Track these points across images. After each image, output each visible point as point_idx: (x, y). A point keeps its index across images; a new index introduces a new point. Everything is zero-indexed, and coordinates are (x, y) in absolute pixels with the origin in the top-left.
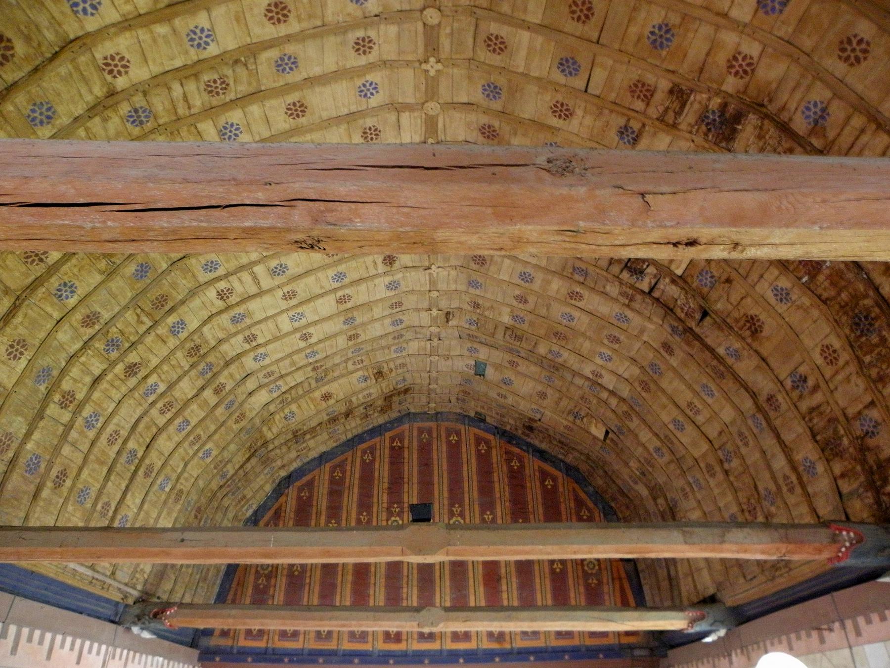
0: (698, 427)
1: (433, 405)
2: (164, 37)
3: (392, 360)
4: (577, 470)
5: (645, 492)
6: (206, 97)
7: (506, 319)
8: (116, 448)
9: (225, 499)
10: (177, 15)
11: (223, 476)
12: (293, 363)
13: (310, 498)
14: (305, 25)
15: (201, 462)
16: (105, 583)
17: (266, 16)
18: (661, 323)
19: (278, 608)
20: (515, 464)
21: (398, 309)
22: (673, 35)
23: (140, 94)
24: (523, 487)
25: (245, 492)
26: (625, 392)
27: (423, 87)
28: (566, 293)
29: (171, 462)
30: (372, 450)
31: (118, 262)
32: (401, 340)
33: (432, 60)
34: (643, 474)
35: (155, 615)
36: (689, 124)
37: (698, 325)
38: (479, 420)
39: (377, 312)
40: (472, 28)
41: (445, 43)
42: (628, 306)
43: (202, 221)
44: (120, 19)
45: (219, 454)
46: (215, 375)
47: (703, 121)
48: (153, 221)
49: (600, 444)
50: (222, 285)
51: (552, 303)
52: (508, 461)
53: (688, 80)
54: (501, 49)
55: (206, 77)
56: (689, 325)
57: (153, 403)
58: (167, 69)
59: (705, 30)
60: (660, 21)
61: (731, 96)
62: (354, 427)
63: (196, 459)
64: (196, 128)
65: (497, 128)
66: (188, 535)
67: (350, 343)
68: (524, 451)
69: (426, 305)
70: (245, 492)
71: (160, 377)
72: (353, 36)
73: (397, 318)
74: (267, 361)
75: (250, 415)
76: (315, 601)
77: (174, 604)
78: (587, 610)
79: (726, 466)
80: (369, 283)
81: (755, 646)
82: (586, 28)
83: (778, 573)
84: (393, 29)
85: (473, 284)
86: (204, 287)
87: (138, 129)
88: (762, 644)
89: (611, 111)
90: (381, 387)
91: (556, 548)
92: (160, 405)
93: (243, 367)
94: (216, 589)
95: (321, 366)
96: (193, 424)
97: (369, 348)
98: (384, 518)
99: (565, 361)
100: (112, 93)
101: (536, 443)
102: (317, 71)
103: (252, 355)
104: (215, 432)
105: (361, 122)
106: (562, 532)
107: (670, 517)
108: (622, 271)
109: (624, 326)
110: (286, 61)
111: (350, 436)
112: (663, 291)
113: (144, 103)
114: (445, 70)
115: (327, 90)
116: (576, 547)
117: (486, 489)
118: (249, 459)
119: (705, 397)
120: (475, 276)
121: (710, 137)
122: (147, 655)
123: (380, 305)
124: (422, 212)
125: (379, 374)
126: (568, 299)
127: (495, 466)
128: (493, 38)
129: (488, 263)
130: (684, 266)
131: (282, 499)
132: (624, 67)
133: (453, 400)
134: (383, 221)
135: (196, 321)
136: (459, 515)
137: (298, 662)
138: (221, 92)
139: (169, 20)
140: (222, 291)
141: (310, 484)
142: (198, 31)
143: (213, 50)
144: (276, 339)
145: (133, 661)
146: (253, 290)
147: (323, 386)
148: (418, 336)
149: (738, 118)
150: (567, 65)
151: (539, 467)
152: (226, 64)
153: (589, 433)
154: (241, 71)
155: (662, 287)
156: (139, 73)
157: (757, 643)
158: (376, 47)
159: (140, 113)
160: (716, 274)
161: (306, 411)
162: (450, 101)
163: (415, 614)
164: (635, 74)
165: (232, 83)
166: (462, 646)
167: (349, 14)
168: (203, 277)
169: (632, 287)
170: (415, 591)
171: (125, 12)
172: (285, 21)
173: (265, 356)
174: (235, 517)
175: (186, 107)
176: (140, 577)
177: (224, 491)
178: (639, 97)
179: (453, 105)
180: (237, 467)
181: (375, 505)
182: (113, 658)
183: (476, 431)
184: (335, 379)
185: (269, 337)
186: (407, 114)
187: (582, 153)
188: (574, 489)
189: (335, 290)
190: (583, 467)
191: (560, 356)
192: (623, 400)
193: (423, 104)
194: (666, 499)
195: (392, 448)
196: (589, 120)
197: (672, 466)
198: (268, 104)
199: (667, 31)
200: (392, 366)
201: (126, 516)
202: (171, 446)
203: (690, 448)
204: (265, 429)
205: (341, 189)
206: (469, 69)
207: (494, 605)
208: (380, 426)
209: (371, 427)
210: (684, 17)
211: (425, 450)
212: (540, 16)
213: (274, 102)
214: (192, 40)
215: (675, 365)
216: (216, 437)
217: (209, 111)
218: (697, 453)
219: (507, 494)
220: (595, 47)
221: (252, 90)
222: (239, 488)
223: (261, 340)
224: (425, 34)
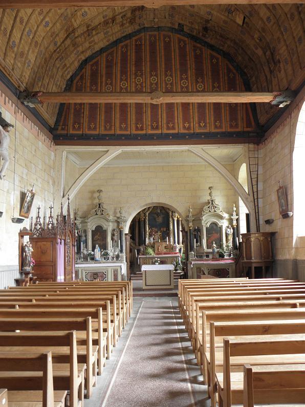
1: (156, 20)
13: (97, 70)
20: (198, 52)
38: (180, 29)
49: (241, 28)
52: (195, 50)
68: (203, 45)
98: (134, 77)
117: (183, 64)
118: (66, 38)
127: (188, 53)
131: (84, 70)
133: (167, 17)
141: (97, 63)
153: (235, 22)
174: (62, 75)
183: (179, 36)
188: (227, 64)
204: (73, 20)
208: (130, 34)
209: (125, 34)
211: (153, 46)
216: (50, 15)
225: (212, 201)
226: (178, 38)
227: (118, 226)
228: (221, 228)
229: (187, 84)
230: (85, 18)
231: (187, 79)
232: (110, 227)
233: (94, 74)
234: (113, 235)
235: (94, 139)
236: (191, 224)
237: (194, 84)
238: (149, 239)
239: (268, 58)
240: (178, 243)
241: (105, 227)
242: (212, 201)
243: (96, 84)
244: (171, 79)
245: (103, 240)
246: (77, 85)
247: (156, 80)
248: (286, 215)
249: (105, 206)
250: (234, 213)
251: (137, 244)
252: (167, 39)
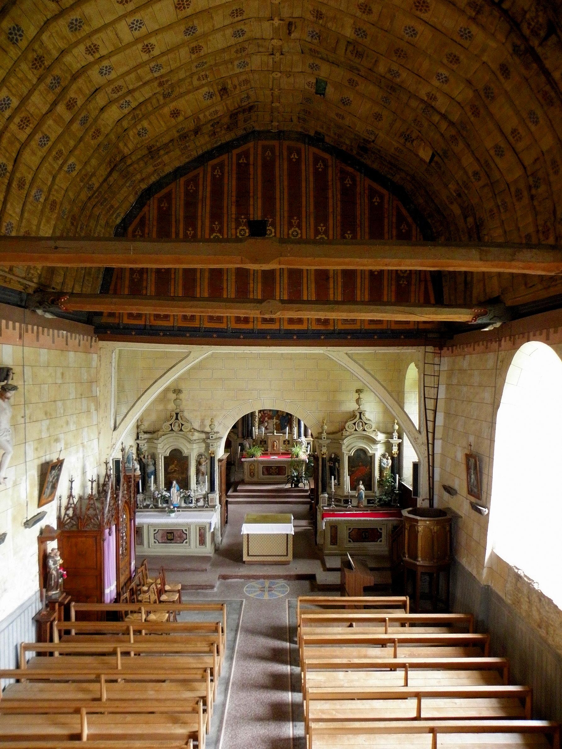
0: (517, 155)
1: (275, 124)
3: (237, 75)
7: (349, 32)
9: (95, 209)
11: (90, 188)
12: (139, 78)
13: (169, 208)
16: (6, 277)
18: (504, 41)
19: (151, 297)
20: (348, 182)
21: (240, 18)
26: (455, 117)
30: (221, 165)
32: (244, 54)
34: (459, 195)
37: (540, 45)
38: (316, 140)
39: (219, 20)
42: (474, 19)
45: (83, 168)
46: (65, 89)
56: (531, 43)
57: (10, 119)
62: (202, 144)
63: (62, 173)
66: (61, 243)
67: (193, 56)
69: (267, 14)
71: (10, 91)
73: (239, 28)
74: (113, 75)
75: (105, 131)
76: (180, 293)
77: (66, 293)
79: (533, 192)
81: (521, 336)
83: (554, 283)
88: (526, 335)
90: (226, 104)
91: (370, 260)
92: (17, 120)
93: (90, 81)
94: (100, 282)
95: (167, 81)
96: (53, 139)
97: (213, 62)
99: (402, 82)
101: (368, 162)
103: (96, 68)
104: (75, 147)
107: (474, 236)
109: (466, 43)
111: (200, 152)
116: (387, 261)
119: (530, 124)
122: (53, 329)
125: (224, 90)
127: (330, 183)
131: (146, 209)
133: (295, 119)
135: (32, 28)
136: (297, 227)
137: (170, 335)
141: (168, 197)
144: (117, 51)
145: (43, 334)
147: (172, 101)
148: (261, 49)
151: (369, 185)
153: (417, 156)
157: (523, 334)
161: (158, 127)
163: (258, 305)
166: (296, 327)
170: (260, 286)
173: (110, 69)
174: (107, 223)
176: (35, 274)
180: (101, 180)
182: (27, 331)
183: (316, 150)
184: (181, 95)
185: (111, 48)
191: (399, 76)
192: (451, 123)
194: (475, 219)
195: (239, 165)
200: (236, 82)
204: (121, 145)
207: (322, 300)
209: (219, 144)
211: (268, 167)
215: (508, 89)
216: (77, 152)
218: (510, 178)
219: (339, 209)
222: (106, 199)
223: (103, 52)
225: (360, 413)
226: (314, 153)
227: (207, 447)
228: (372, 457)
230: (143, 138)
231: (326, 232)
232: (193, 451)
233: (164, 217)
234: (199, 463)
235: (164, 335)
236: (324, 450)
238: (259, 428)
239: (469, 227)
240: (306, 436)
241: (186, 452)
242: (360, 413)
244: (299, 232)
245: (183, 473)
248: (478, 491)
249: (186, 414)
250: (395, 435)
251: (240, 435)
252: (294, 156)
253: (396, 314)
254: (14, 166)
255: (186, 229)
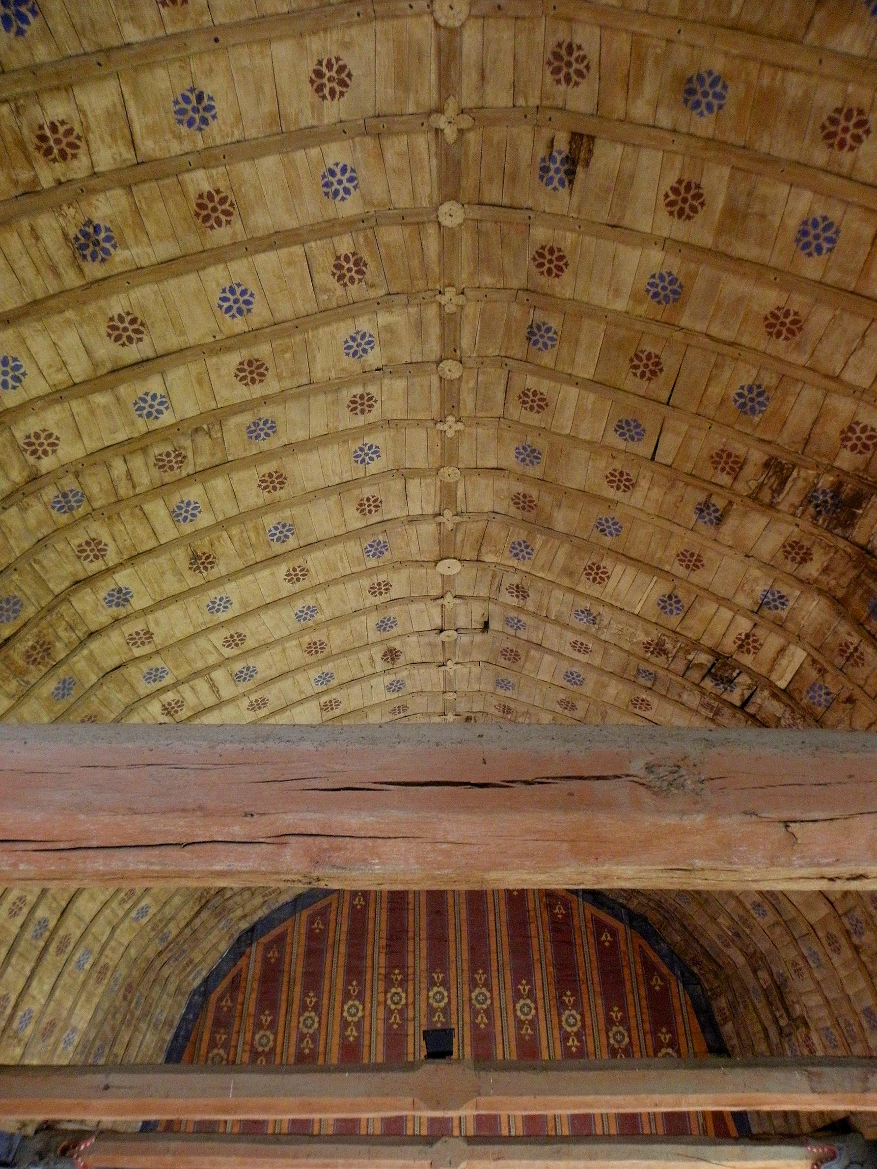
2: (105, 407)
4: (645, 919)
5: (740, 960)
6: (156, 473)
8: (20, 920)
9: (165, 968)
10: (123, 381)
13: (280, 961)
14: (287, 384)
15: (134, 924)
17: (236, 376)
21: (402, 715)
22: (768, 399)
23: (71, 475)
24: (570, 944)
25: (193, 955)
27: (438, 450)
28: (628, 700)
29: (94, 930)
31: (33, 681)
33: (450, 419)
34: (737, 934)
35: (64, 1151)
36: (792, 505)
40: (503, 382)
41: (468, 401)
42: (712, 720)
43: (152, 864)
44: (48, 390)
45: (159, 911)
47: (810, 502)
48: (84, 863)
50: (169, 697)
51: (609, 711)
53: (789, 453)
54: (540, 406)
55: (156, 450)
58: (106, 444)
59: (810, 394)
60: (750, 381)
61: (847, 473)
63: (127, 922)
64: (142, 509)
65: (535, 497)
69: (439, 708)
70: (193, 955)
72: (346, 395)
78: (667, 1142)
79: (856, 940)
80: (364, 685)
82: (652, 385)
84: (399, 384)
85: (502, 684)
86: (146, 700)
87: (66, 516)
89: (687, 484)
100: (34, 478)
102: (301, 435)
105: (356, 492)
106: (637, 1074)
108: (703, 678)
110: (261, 426)
112: (761, 706)
113: (75, 486)
114: (467, 430)
115: (313, 457)
117: (520, 948)
118: (198, 913)
120: (504, 674)
121: (821, 521)
123: (378, 710)
124: (467, 848)
126: (631, 707)
127: (532, 913)
128: (530, 394)
129: (523, 659)
130: (788, 677)
131: (242, 962)
132: (703, 434)
134: (412, 861)
136: (484, 985)
138: (176, 466)
139: (112, 389)
140: (169, 704)
141: (281, 939)
142: (149, 398)
143: (167, 418)
146: (211, 700)
149: (857, 500)
150: (629, 428)
152: (183, 434)
154: (204, 442)
155: (759, 701)
156: (70, 451)
158: (377, 405)
159: (70, 498)
160: (832, 690)
162: (473, 465)
163: (427, 1148)
164: (717, 441)
165: (190, 455)
167: (343, 369)
168: (144, 688)
169: (718, 698)
171: (56, 382)
172: (261, 381)
175: (130, 487)
177: (164, 957)
178: (723, 469)
179: (478, 470)
180: (183, 924)
181: (369, 971)
186: (417, 481)
187: (694, 751)
188: (640, 946)
189: (319, 694)
190: (654, 917)
193: (438, 469)
196: (656, 493)
197: (778, 930)
198: (236, 477)
199: (760, 394)
201: (30, 1011)
202: (94, 907)
203: (802, 911)
205: (353, 821)
206: (499, 428)
210: (782, 377)
212: (592, 370)
213: (244, 474)
214: (141, 409)
217: (159, 490)
219: (549, 954)
220: (664, 409)
221: (216, 460)
222: (184, 951)
224: (441, 389)
229: (533, 1012)
231: (531, 995)
233: (271, 975)
237: (554, 1012)
243: (273, 1007)
244: (488, 994)
246: (219, 1008)
247: (446, 1000)
253: (673, 1160)
254: (59, 920)
255: (305, 994)
